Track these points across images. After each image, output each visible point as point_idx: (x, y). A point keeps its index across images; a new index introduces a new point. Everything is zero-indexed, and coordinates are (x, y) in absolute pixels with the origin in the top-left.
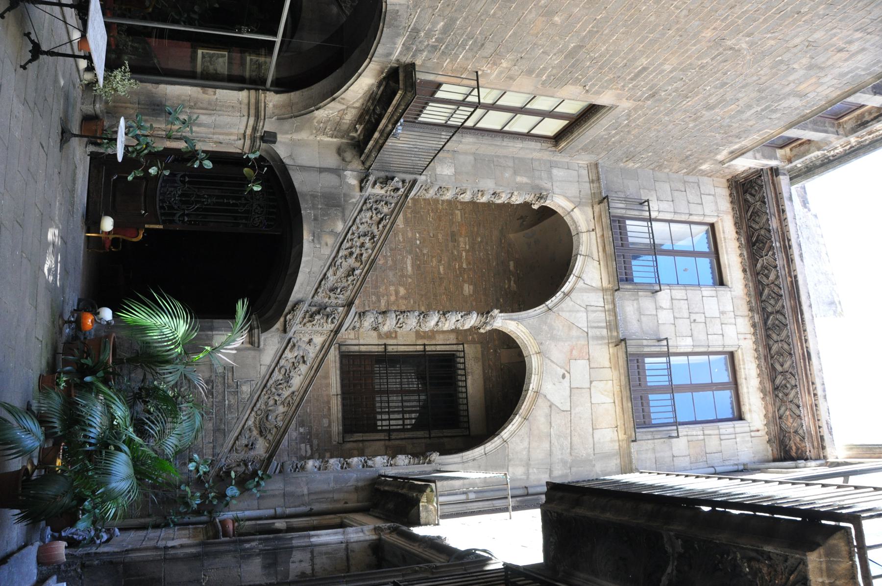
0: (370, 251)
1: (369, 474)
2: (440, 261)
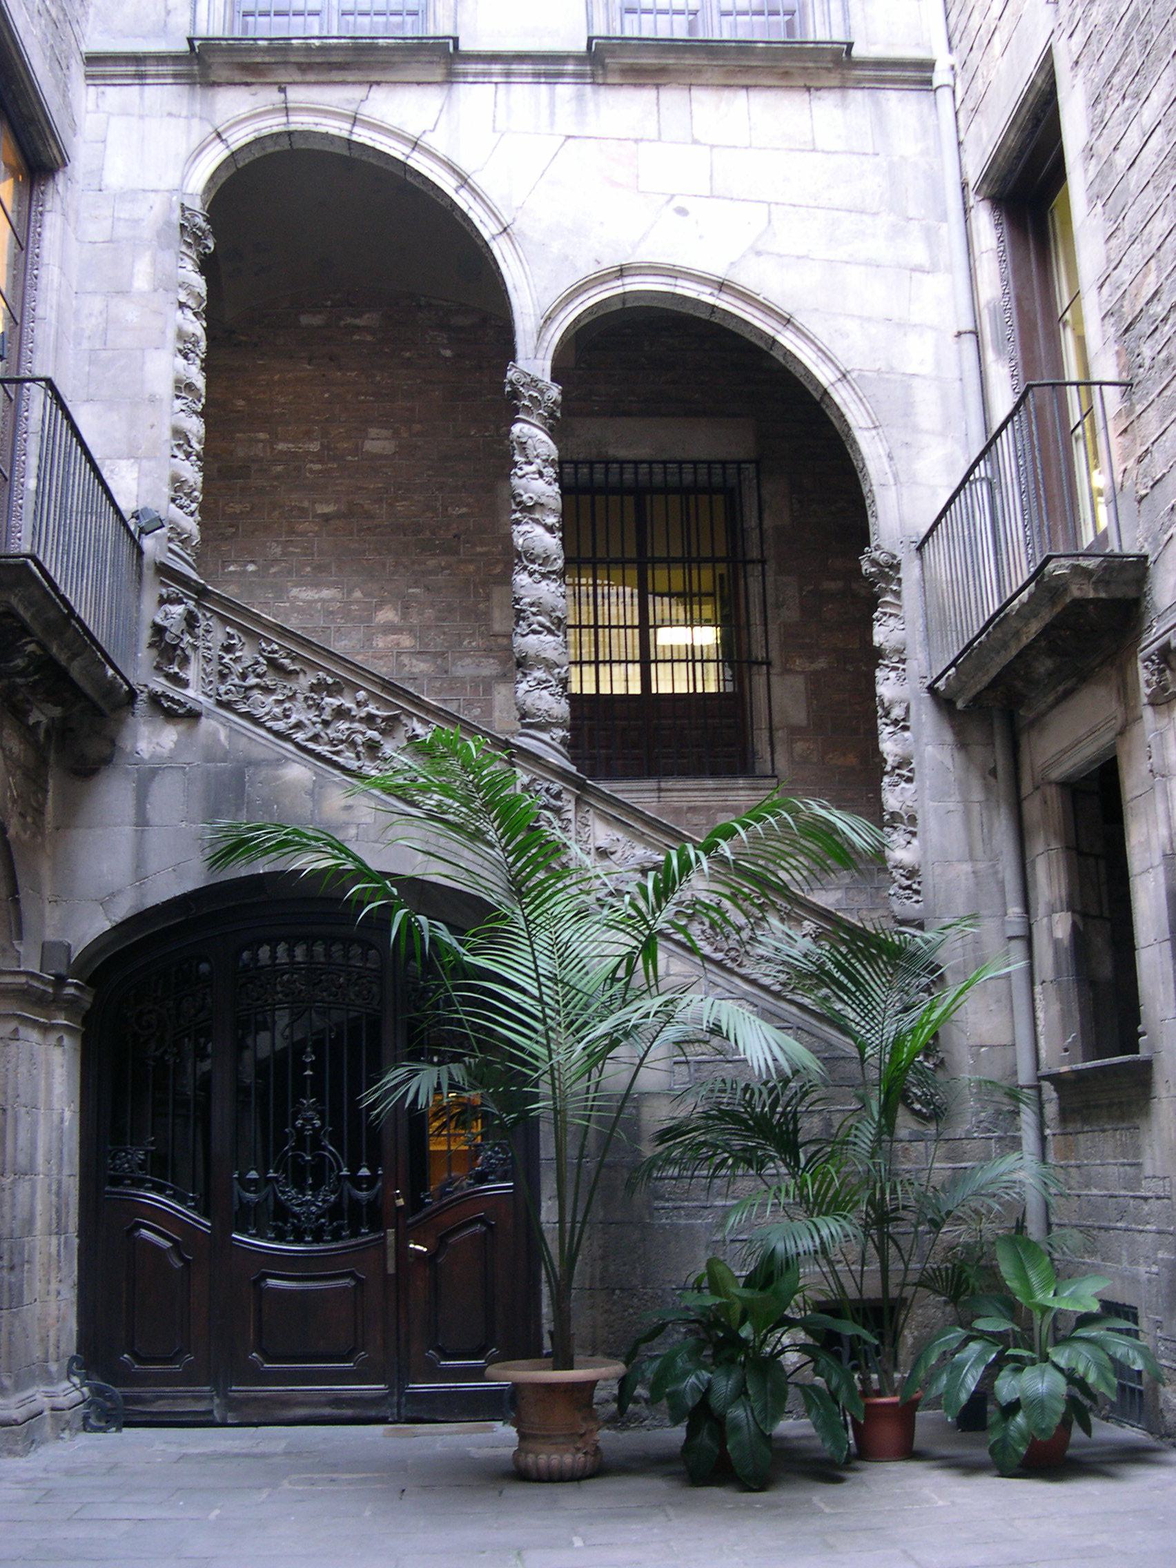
0: (362, 695)
1: (925, 716)
2: (303, 512)
